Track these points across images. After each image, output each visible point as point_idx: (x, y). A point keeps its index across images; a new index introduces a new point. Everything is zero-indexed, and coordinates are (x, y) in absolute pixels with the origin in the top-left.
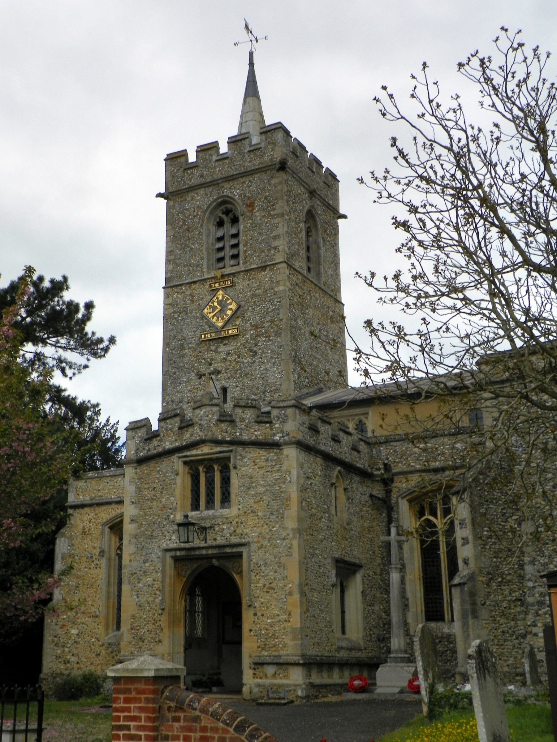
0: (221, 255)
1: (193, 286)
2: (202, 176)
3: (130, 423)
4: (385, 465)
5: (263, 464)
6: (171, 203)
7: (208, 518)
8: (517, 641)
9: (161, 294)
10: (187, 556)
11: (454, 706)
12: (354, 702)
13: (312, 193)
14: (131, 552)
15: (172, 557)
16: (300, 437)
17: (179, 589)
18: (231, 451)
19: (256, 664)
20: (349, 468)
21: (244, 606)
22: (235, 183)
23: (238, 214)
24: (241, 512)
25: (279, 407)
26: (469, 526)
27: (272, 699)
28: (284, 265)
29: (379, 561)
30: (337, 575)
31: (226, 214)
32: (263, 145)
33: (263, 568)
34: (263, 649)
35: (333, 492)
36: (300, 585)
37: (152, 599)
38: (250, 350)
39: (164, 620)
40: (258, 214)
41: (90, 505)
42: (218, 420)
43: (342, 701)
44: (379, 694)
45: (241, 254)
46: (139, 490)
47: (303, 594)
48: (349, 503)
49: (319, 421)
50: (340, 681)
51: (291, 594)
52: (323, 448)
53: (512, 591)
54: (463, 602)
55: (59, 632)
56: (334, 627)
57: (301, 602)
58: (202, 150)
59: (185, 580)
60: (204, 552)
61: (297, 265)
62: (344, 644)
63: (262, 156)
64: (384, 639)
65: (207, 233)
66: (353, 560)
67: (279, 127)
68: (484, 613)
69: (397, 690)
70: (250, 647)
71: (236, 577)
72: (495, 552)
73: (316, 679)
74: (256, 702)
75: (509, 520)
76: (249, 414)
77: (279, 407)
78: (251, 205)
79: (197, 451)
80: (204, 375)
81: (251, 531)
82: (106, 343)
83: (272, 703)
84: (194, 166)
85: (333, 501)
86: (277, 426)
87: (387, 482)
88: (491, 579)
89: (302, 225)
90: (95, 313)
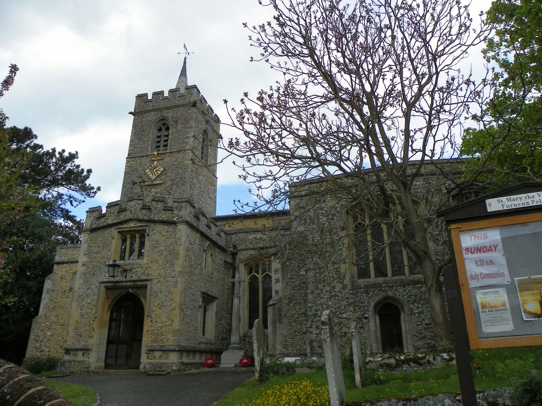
0: (158, 144)
1: (142, 158)
2: (153, 106)
3: (90, 208)
4: (234, 245)
5: (165, 234)
6: (136, 117)
7: (129, 264)
8: (301, 336)
9: (125, 160)
10: (114, 286)
11: (276, 373)
12: (206, 373)
13: (207, 122)
14: (80, 283)
15: (105, 287)
16: (188, 219)
17: (107, 306)
18: (147, 226)
19: (149, 350)
20: (215, 244)
21: (145, 317)
22: (170, 110)
23: (169, 126)
24: (149, 261)
25: (178, 202)
26: (280, 272)
27: (157, 371)
28: (190, 151)
29: (226, 296)
30: (202, 302)
31: (164, 126)
32: (186, 94)
33: (159, 294)
34: (155, 342)
35: (205, 255)
36: (180, 304)
37: (89, 311)
38: (168, 192)
39: (95, 324)
40: (179, 126)
41: (67, 263)
42: (141, 208)
43: (200, 373)
44: (222, 368)
45: (169, 145)
46: (90, 246)
47: (182, 310)
48: (212, 263)
49: (200, 214)
50: (199, 361)
51: (174, 309)
52: (201, 229)
53: (300, 308)
54: (274, 314)
55: (40, 333)
56: (198, 330)
57: (180, 314)
58: (155, 94)
59: (111, 300)
60: (124, 284)
61: (197, 153)
62: (203, 341)
63: (185, 99)
64: (225, 338)
65: (152, 135)
66: (212, 294)
67: (195, 87)
68: (285, 321)
69: (233, 365)
70: (146, 340)
71: (142, 299)
72: (293, 287)
73: (185, 360)
74: (147, 374)
75: (302, 270)
76: (160, 205)
77: (178, 202)
78: (177, 122)
79: (127, 225)
80: (136, 183)
81: (154, 272)
82: (95, 190)
83: (158, 373)
84: (150, 101)
85: (204, 260)
86: (176, 212)
87: (234, 255)
88: (290, 302)
89: (201, 135)
90: (92, 175)
